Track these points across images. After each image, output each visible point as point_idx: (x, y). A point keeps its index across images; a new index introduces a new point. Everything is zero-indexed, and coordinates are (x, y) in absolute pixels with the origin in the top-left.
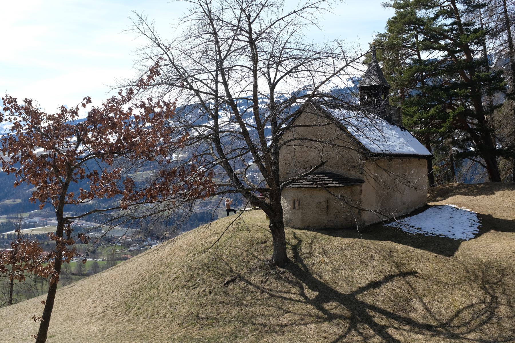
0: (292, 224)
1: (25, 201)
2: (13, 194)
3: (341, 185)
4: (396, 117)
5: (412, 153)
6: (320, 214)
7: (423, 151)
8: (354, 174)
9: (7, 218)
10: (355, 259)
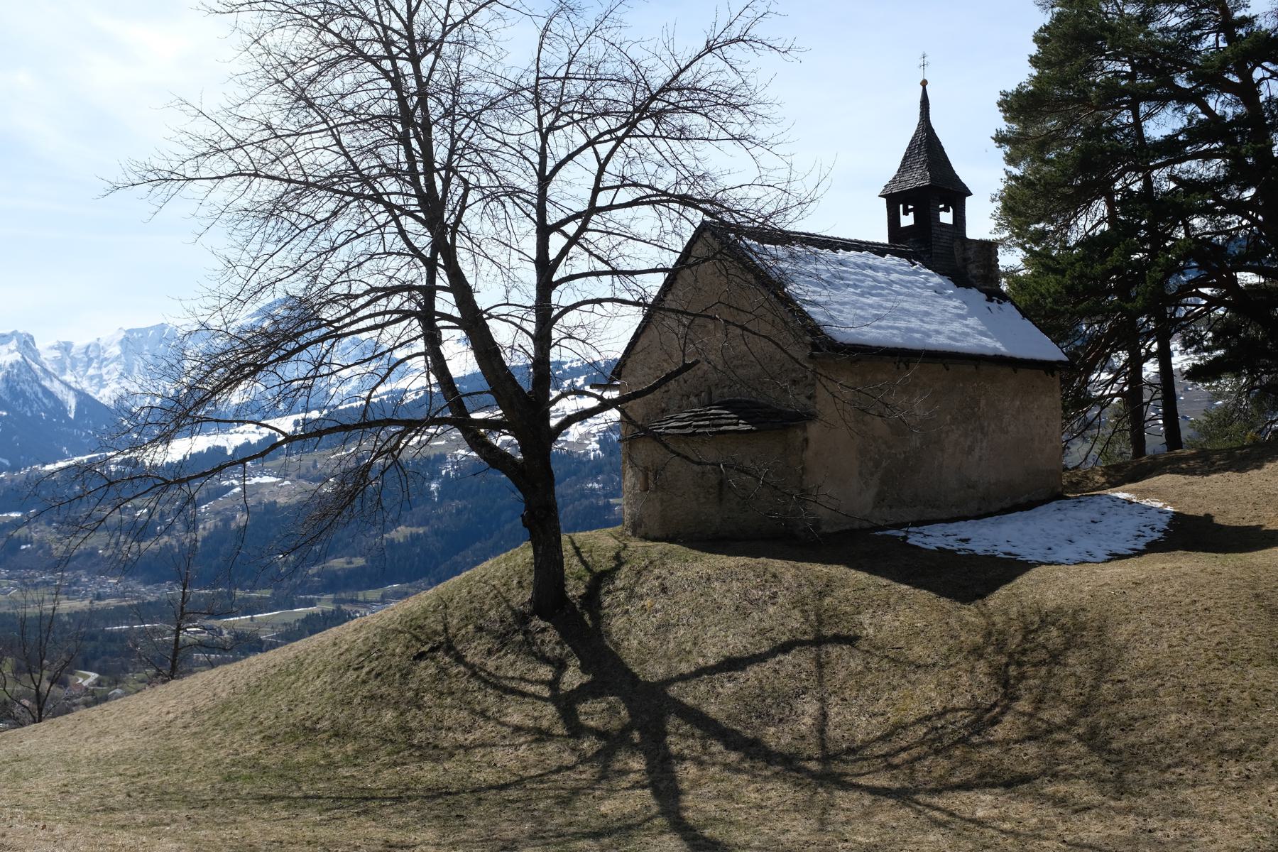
0: (642, 530)
2: (347, 545)
3: (749, 427)
4: (977, 267)
5: (991, 353)
6: (703, 500)
7: (1046, 349)
8: (795, 400)
9: (335, 601)
10: (726, 601)
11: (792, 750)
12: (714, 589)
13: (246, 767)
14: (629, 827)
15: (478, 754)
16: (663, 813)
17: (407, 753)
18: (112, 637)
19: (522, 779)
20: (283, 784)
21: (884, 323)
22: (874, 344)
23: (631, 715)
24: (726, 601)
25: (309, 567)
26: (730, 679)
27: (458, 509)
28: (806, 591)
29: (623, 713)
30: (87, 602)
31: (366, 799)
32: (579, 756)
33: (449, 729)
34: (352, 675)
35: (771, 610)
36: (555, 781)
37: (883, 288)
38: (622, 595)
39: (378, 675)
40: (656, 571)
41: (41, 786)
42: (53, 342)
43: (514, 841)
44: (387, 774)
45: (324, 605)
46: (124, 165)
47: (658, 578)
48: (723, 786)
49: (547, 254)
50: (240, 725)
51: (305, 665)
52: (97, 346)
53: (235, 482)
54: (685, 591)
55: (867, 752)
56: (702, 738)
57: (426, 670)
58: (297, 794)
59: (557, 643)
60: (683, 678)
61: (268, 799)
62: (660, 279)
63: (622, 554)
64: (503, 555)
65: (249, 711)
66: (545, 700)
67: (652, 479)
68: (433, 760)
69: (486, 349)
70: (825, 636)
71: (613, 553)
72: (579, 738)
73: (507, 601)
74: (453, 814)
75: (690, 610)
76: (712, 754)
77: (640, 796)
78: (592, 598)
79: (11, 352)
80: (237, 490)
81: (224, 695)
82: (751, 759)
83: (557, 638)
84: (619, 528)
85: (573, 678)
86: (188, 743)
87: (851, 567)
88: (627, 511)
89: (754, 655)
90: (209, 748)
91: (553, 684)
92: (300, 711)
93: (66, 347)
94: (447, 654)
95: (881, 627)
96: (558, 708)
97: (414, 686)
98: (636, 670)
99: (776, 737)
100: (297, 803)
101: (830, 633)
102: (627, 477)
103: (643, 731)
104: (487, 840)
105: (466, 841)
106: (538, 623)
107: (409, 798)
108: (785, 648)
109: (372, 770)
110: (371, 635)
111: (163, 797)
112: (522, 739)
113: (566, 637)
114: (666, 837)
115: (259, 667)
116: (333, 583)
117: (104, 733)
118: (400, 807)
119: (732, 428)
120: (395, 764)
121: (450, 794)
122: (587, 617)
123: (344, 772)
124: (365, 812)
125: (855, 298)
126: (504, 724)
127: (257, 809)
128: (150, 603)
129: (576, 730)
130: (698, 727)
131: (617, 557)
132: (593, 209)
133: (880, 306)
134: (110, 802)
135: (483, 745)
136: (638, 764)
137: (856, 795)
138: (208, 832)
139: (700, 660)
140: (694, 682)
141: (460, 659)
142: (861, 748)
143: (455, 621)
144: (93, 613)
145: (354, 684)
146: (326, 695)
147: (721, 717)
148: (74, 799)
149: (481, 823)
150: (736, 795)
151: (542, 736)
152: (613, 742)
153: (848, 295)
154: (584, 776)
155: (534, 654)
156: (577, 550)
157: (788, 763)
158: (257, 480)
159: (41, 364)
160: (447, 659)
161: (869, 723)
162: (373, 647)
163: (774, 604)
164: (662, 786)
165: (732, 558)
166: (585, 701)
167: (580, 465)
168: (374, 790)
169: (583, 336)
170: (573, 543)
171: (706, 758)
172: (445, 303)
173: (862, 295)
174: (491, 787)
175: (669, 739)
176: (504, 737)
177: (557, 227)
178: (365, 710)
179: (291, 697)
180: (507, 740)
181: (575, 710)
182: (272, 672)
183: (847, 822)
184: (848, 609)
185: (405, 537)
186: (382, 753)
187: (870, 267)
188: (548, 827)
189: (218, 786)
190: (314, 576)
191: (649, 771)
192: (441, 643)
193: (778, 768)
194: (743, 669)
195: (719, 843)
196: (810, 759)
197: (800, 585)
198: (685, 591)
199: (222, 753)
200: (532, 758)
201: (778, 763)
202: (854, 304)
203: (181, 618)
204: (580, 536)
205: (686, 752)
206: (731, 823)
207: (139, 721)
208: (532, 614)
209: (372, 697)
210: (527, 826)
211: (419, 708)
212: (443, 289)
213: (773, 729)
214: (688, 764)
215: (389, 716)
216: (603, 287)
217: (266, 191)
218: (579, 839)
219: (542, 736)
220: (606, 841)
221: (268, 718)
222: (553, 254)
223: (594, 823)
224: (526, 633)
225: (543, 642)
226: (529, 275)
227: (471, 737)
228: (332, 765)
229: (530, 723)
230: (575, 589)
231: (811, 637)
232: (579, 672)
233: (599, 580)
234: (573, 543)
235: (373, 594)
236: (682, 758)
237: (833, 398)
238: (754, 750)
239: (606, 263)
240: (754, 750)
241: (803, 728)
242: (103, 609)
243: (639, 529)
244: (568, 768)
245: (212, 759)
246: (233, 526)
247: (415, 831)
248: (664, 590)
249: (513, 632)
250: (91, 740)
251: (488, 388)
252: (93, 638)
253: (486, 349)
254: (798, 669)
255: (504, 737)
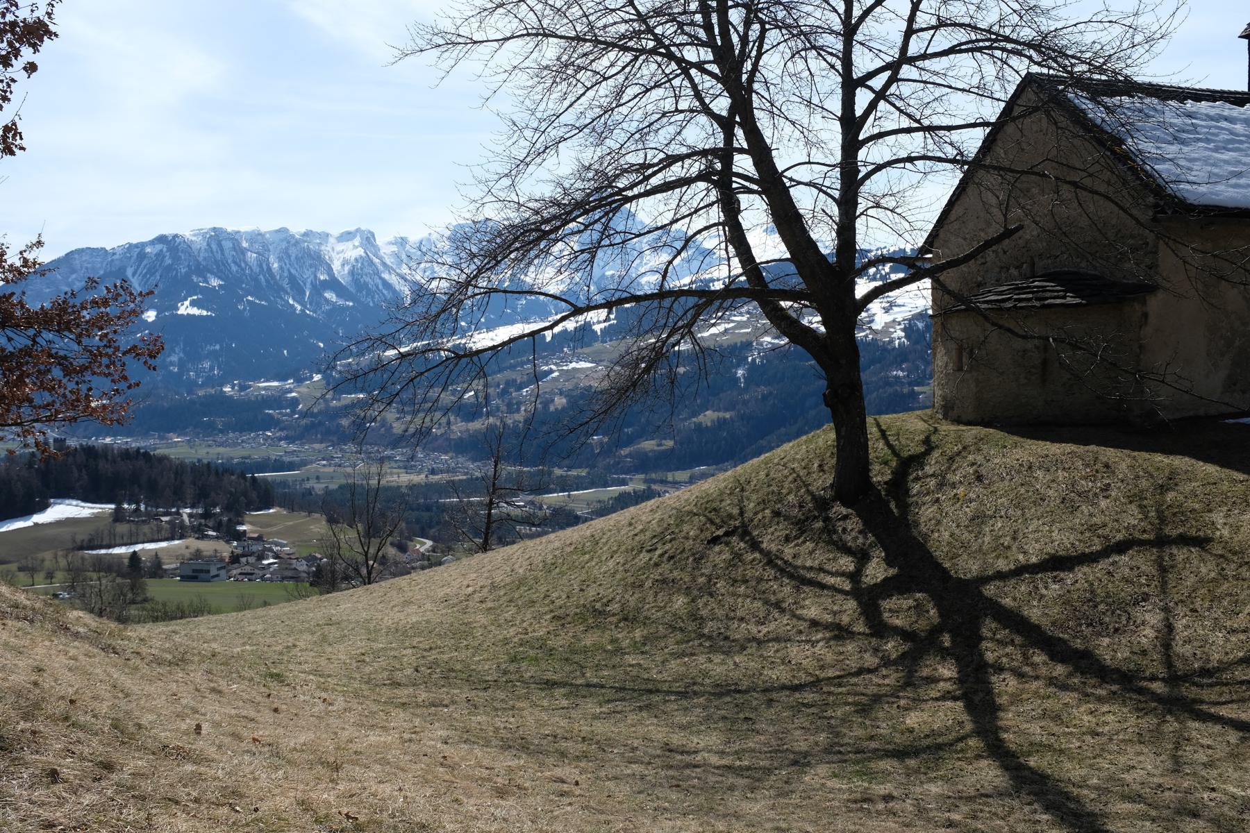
1: (681, 444)
9: (646, 481)
10: (1051, 492)
11: (1132, 666)
12: (1036, 479)
13: (533, 648)
14: (939, 747)
15: (771, 650)
16: (979, 732)
17: (696, 642)
18: (443, 509)
19: (819, 680)
20: (567, 668)
21: (1243, 181)
22: (1230, 205)
23: (941, 615)
24: (1051, 492)
25: (621, 448)
26: (1055, 580)
27: (763, 396)
28: (1144, 483)
29: (932, 612)
30: (423, 476)
31: (650, 691)
32: (882, 658)
33: (742, 619)
34: (644, 556)
35: (1103, 504)
36: (856, 685)
37: (1241, 142)
38: (932, 483)
39: (671, 558)
40: (971, 457)
41: (342, 652)
42: (391, 238)
43: (806, 755)
44: (674, 664)
45: (635, 484)
46: (412, 31)
47: (973, 464)
48: (1048, 704)
49: (853, 110)
50: (533, 602)
51: (600, 545)
52: (429, 240)
53: (553, 367)
54: (1003, 479)
55: (1227, 676)
56: (1022, 646)
57: (720, 555)
58: (580, 681)
59: (860, 532)
60: (1001, 576)
61: (550, 685)
62: (979, 134)
63: (933, 438)
64: (804, 438)
65: (543, 589)
66: (846, 593)
67: (967, 357)
68: (723, 653)
69: (788, 221)
70: (1168, 537)
71: (922, 437)
72: (882, 637)
73: (807, 486)
74: (741, 716)
75: (1010, 502)
76: (1034, 666)
77: (951, 709)
78: (899, 484)
79: (355, 247)
80: (556, 374)
81: (521, 571)
82: (1082, 673)
83: (860, 526)
84: (929, 411)
85: (876, 571)
86: (482, 619)
87: (1198, 458)
88: (938, 392)
89: (1083, 554)
90: (499, 626)
91: (855, 577)
92: (591, 593)
93: (403, 242)
94: (742, 540)
95: (1238, 528)
96: (860, 603)
97: (706, 571)
98: (947, 565)
99: (1111, 650)
100: (579, 691)
101: (1175, 533)
102: (939, 356)
103: (954, 634)
104: (776, 751)
105: (753, 751)
106: (839, 509)
107: (695, 693)
108: (1121, 547)
109: (659, 659)
110: (666, 516)
111: (449, 675)
112: (820, 636)
113: (869, 525)
114: (984, 763)
115: (557, 544)
116: (644, 464)
117: (408, 603)
118: (685, 703)
119: (1058, 301)
120: (683, 654)
121: (739, 692)
122: (893, 505)
123: (631, 659)
124: (648, 707)
125: (1207, 153)
126: (799, 618)
127: (537, 695)
128: (477, 479)
129: (879, 630)
130: (1018, 632)
131: (927, 441)
132: (905, 58)
133: (1239, 162)
134: (398, 676)
135: (777, 640)
136: (947, 671)
137: (1218, 728)
138: (484, 718)
139: (1021, 557)
140: (1013, 581)
141: (755, 545)
142: (1218, 670)
143: (752, 505)
144: (429, 486)
145: (646, 566)
146: (618, 576)
147: (1045, 623)
148: (368, 669)
149: (771, 730)
150: (1065, 717)
151: (841, 633)
152: (920, 646)
153: (1197, 150)
154: (887, 681)
155: (834, 543)
156: (883, 434)
157: (1125, 682)
158: (573, 365)
159: (381, 259)
160: (742, 545)
161: (1228, 640)
162: (667, 529)
163: (1106, 497)
164: (977, 699)
165: (1058, 445)
166: (890, 596)
167: (884, 353)
168: (659, 682)
169: (892, 204)
170: (878, 425)
171: (1027, 669)
172: (744, 164)
173: (1216, 150)
174: (784, 687)
175: (984, 644)
176: (800, 632)
177: (863, 82)
178: (656, 594)
179: (584, 577)
180: (801, 635)
181: (877, 607)
182: (568, 549)
183: (1209, 765)
184: (1197, 506)
185: (713, 421)
186: (671, 641)
187: (1226, 119)
188: (846, 740)
189: (503, 666)
190: (626, 456)
191: (960, 681)
192: (736, 528)
193: (1114, 688)
194: (1071, 569)
195: (1048, 777)
196: (1153, 678)
197: (1137, 477)
198: (1003, 479)
199: (512, 631)
200: (830, 657)
201: (1114, 682)
202: (1206, 161)
203: (494, 493)
204: (885, 419)
205: (1004, 660)
206: (1061, 751)
207: (441, 593)
208: (834, 501)
209: (664, 581)
210: (822, 737)
211: (711, 595)
212: (741, 151)
213: (1107, 641)
214: (1007, 675)
215: (680, 602)
216: (915, 144)
217: (551, 50)
218: (881, 758)
219: (841, 633)
220: (912, 763)
221: (560, 597)
222: (859, 112)
223: (899, 739)
224: (827, 520)
225: (844, 530)
226: (833, 135)
227: (764, 630)
228: (619, 651)
229: (828, 618)
230: (880, 475)
231: (1152, 537)
232: (884, 565)
233: (907, 465)
234: (878, 425)
235: (682, 475)
236: (1000, 669)
237: (1177, 265)
238: (1084, 663)
239: (918, 121)
240: (1084, 663)
241: (1144, 640)
242: (437, 483)
243: (951, 412)
244: (869, 671)
245: (501, 637)
246: (552, 408)
247: (699, 732)
248: (979, 478)
249: (812, 519)
250: (396, 609)
251: (788, 255)
252: (428, 508)
253: (788, 221)
254: (1136, 572)
255: (800, 632)
